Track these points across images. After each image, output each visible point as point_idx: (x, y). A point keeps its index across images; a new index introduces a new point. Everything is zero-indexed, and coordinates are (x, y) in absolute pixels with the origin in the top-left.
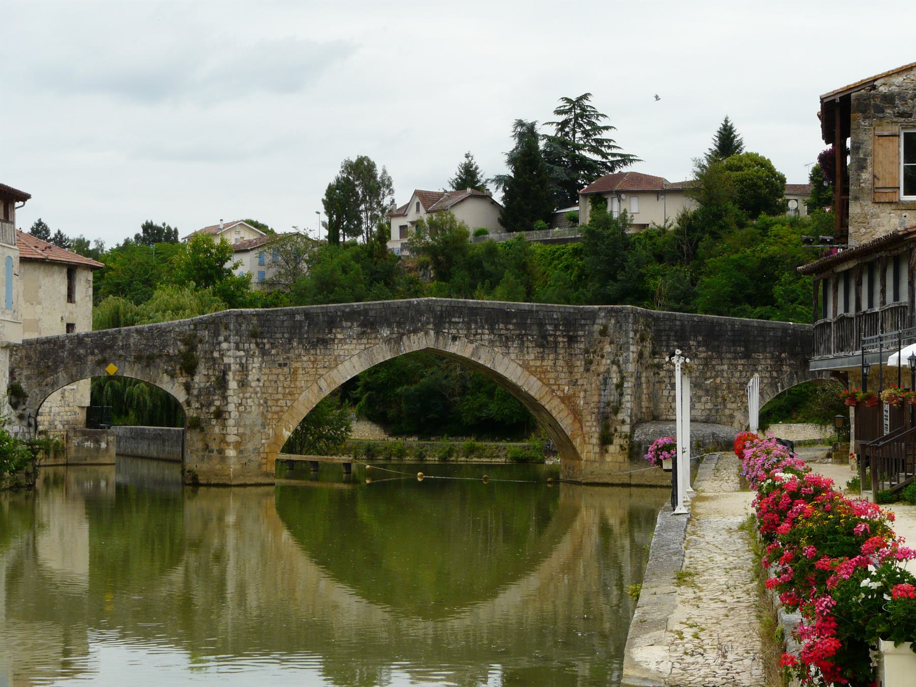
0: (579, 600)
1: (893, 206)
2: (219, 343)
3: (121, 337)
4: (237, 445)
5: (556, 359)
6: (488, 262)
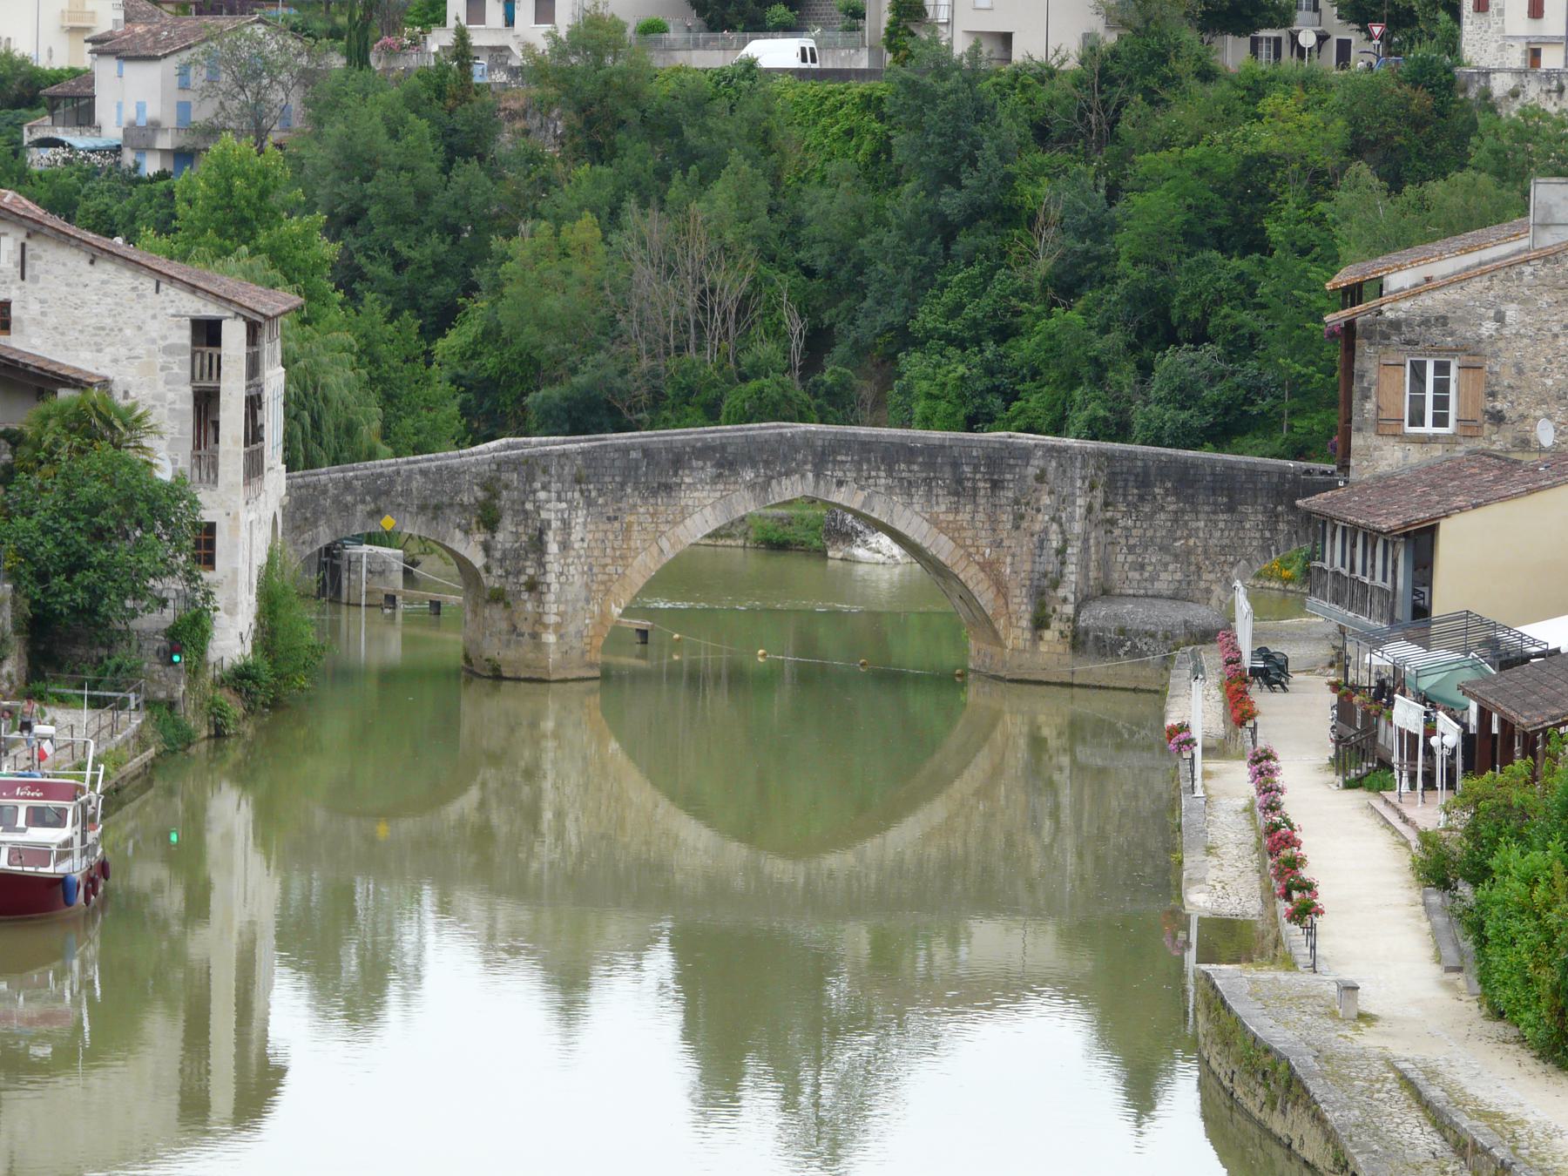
0: (998, 841)
1: (1397, 439)
2: (534, 492)
3: (400, 480)
4: (558, 626)
5: (975, 512)
6: (692, 126)
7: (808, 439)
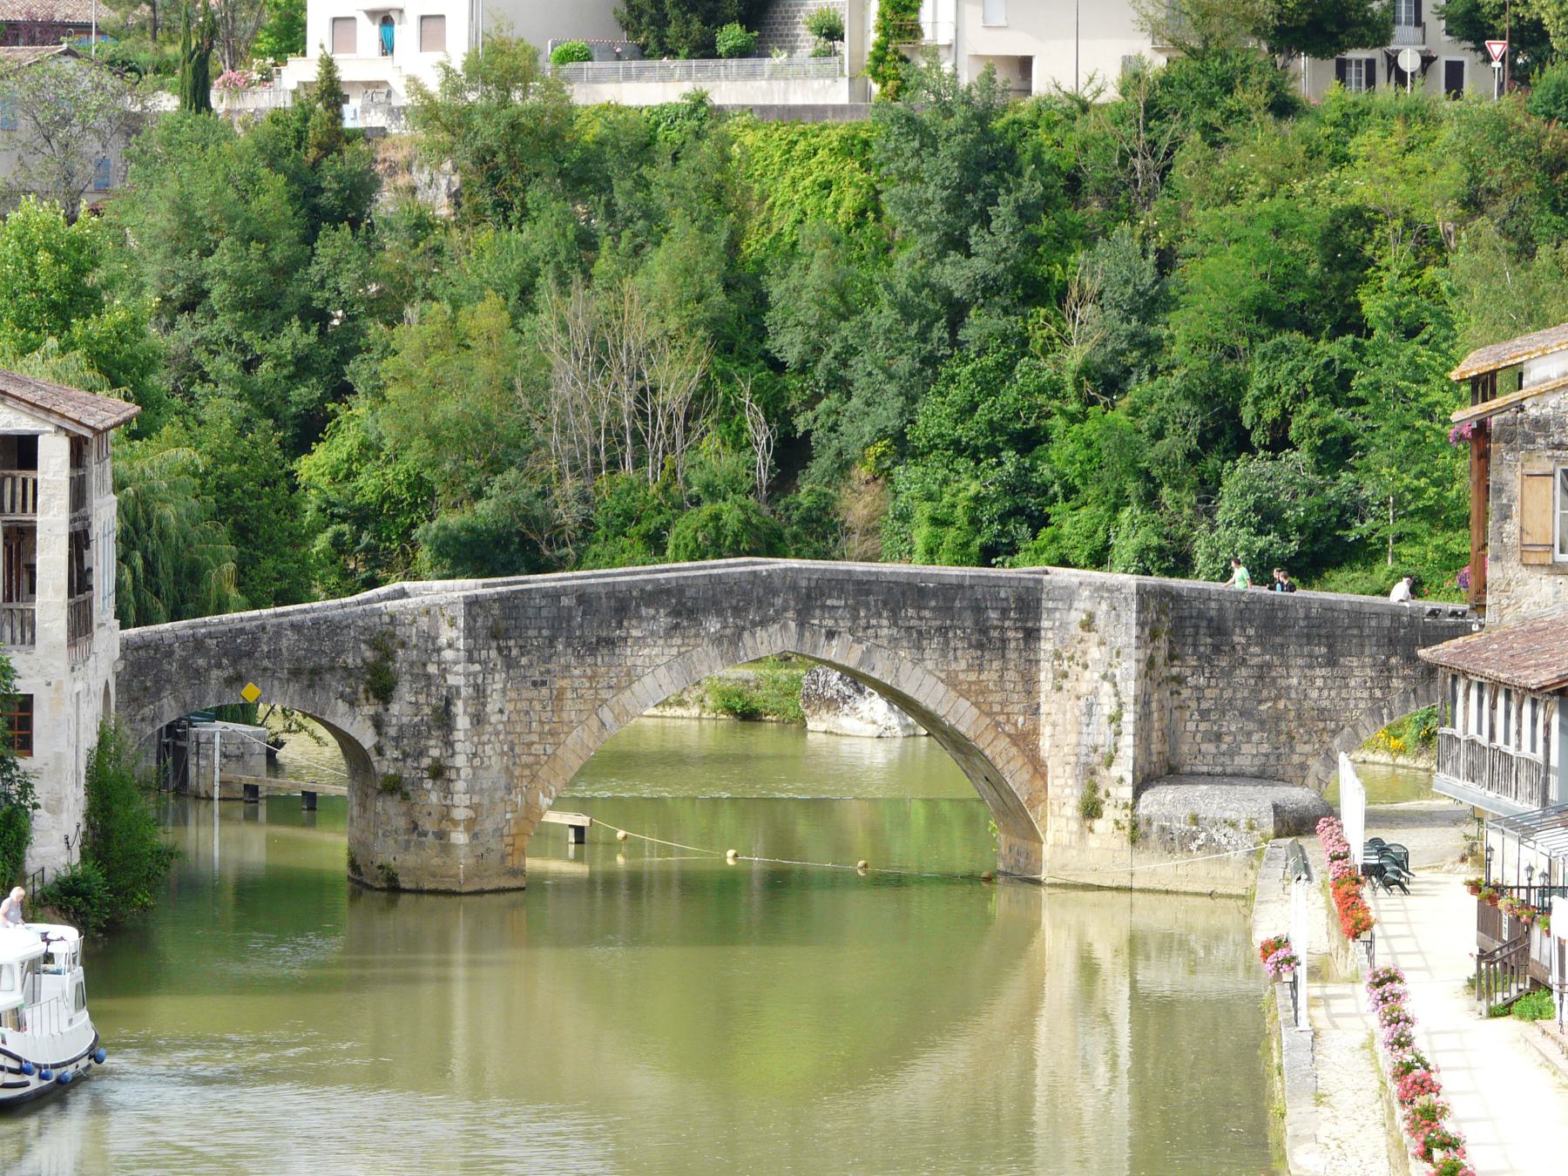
7: (790, 580)
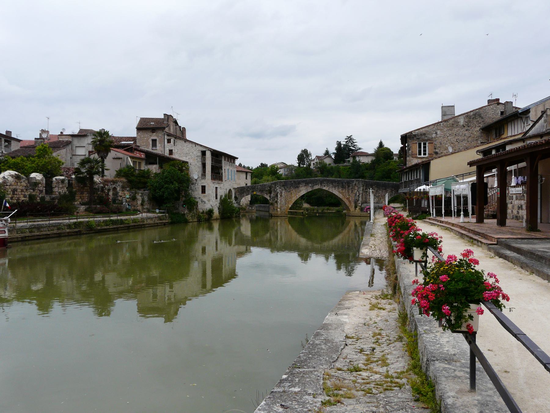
0: (350, 240)
7: (319, 180)
